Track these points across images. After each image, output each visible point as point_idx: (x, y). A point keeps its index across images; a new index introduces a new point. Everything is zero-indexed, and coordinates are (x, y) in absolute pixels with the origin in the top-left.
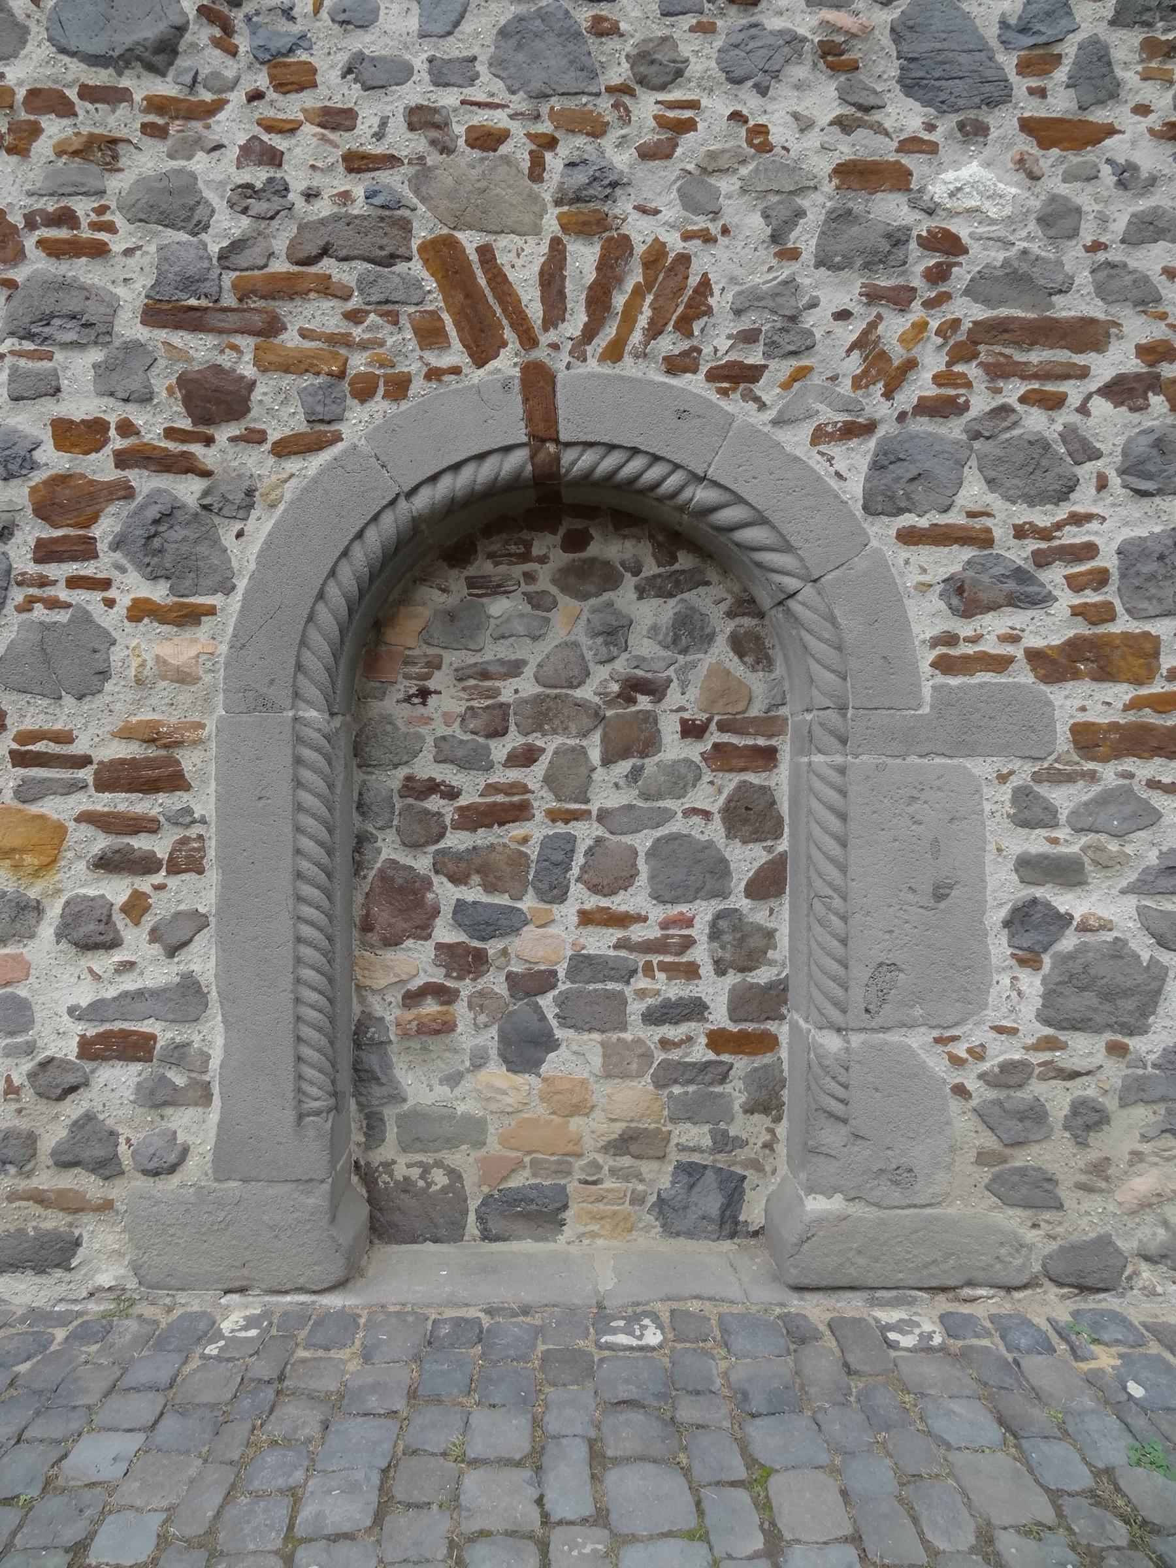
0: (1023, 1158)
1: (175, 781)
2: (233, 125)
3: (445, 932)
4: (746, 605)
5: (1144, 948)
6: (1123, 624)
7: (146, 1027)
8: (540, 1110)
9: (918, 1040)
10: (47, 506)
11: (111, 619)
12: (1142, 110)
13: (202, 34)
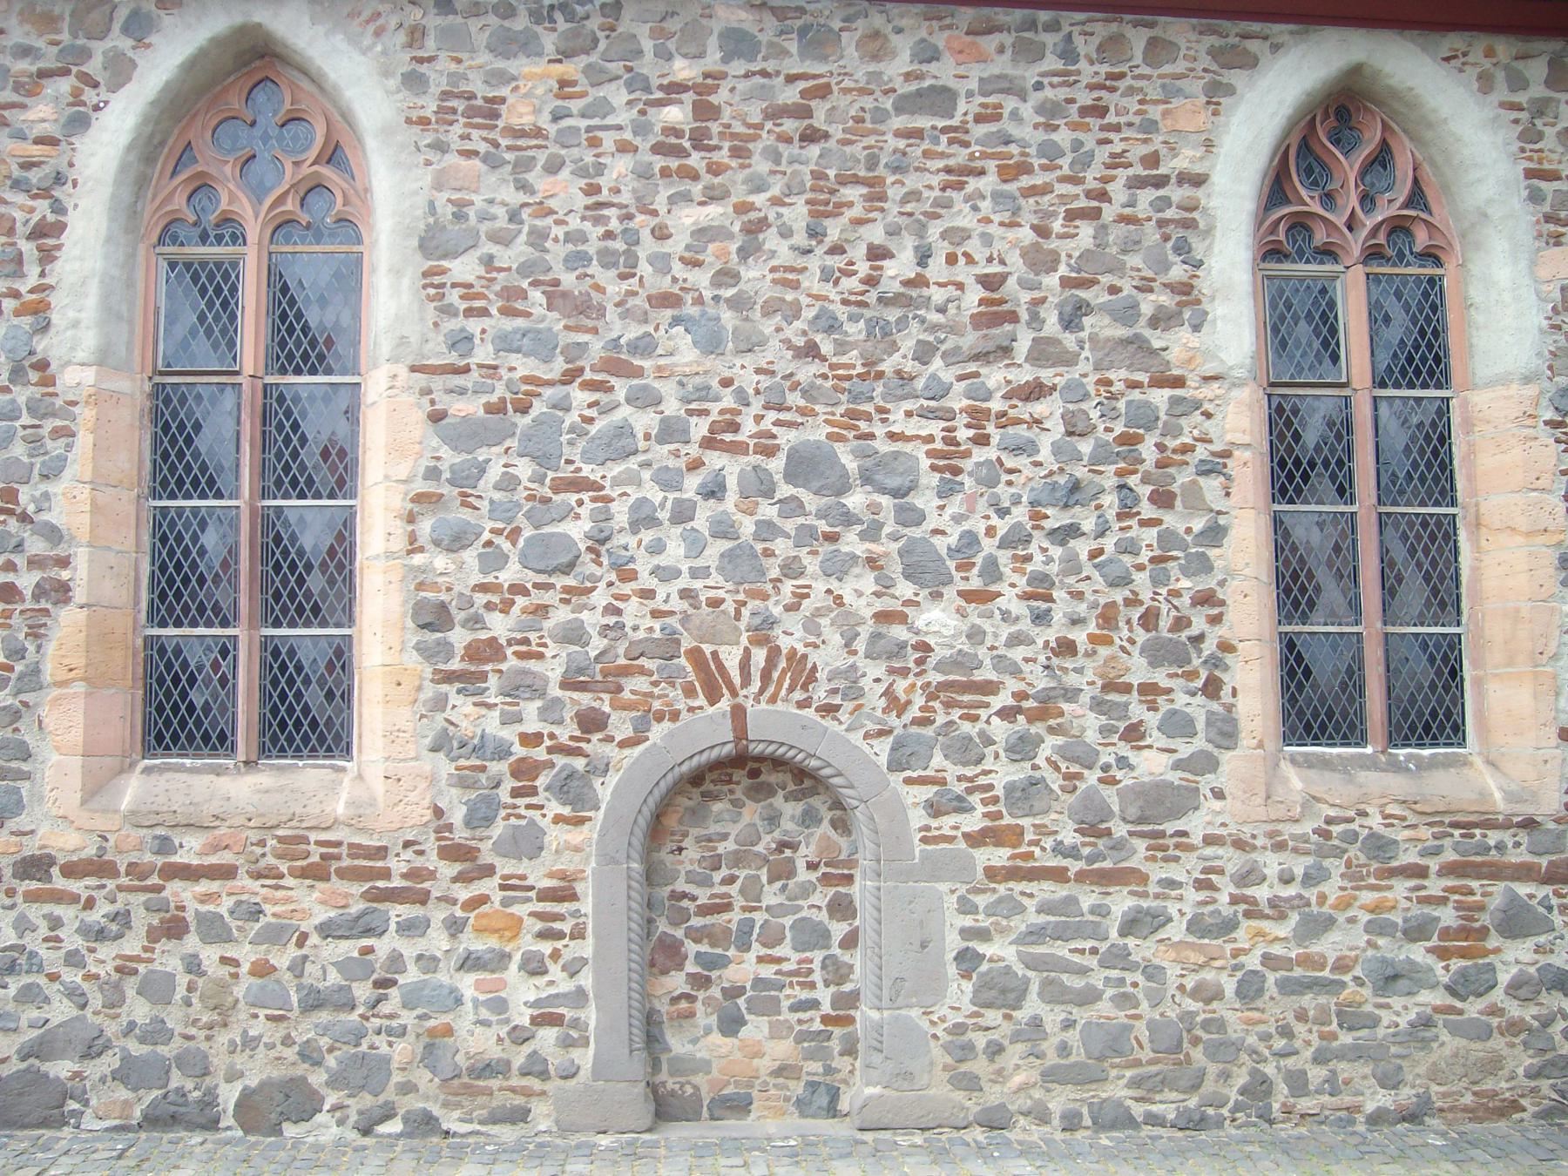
0: (964, 1068)
1: (573, 897)
2: (600, 598)
3: (691, 967)
4: (837, 805)
5: (1019, 969)
6: (1007, 820)
7: (560, 1010)
8: (738, 1055)
9: (915, 1013)
10: (516, 773)
11: (545, 823)
12: (1013, 585)
13: (587, 557)
